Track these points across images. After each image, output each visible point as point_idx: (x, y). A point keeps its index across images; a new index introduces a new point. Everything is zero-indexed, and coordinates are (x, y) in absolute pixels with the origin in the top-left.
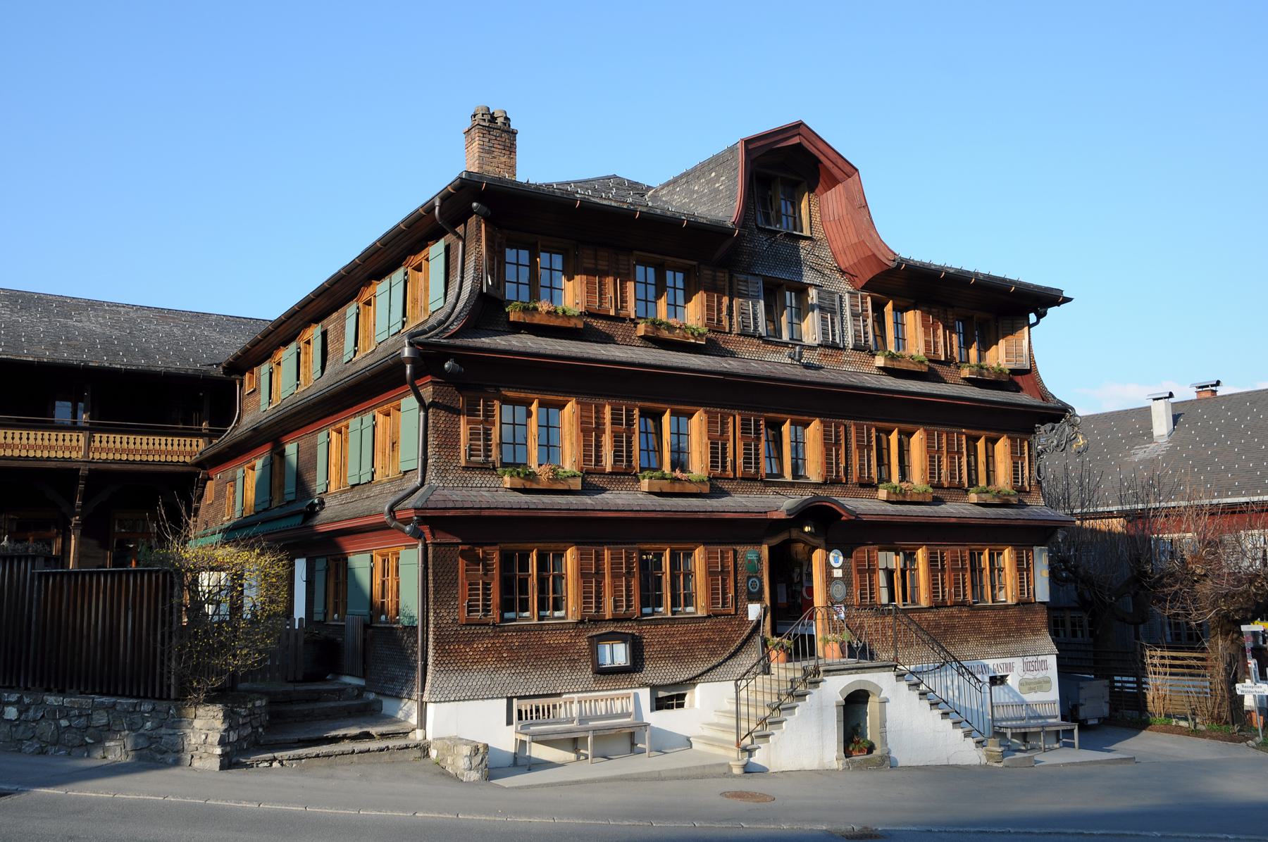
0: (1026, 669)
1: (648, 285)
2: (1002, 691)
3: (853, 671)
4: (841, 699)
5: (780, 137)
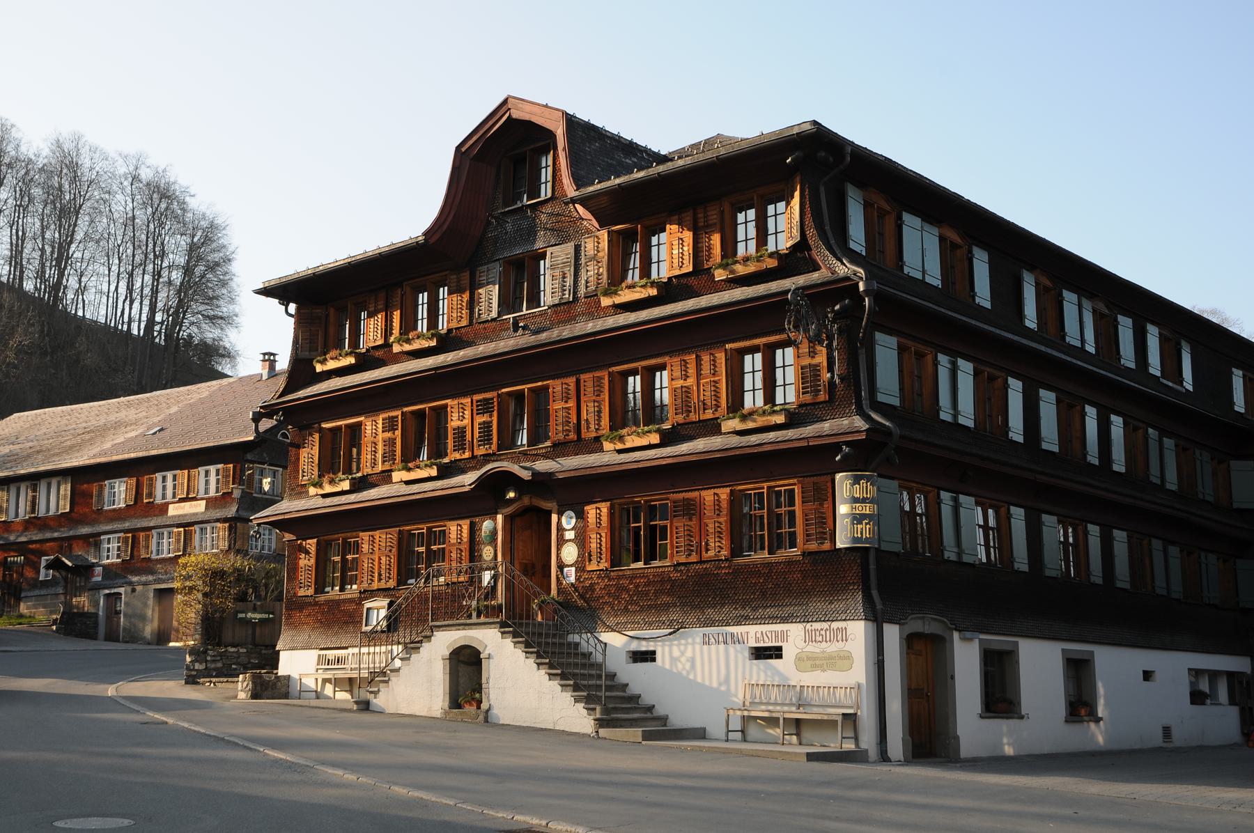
0: (810, 638)
1: (774, 217)
2: (755, 668)
3: (461, 627)
4: (447, 653)
5: (491, 123)
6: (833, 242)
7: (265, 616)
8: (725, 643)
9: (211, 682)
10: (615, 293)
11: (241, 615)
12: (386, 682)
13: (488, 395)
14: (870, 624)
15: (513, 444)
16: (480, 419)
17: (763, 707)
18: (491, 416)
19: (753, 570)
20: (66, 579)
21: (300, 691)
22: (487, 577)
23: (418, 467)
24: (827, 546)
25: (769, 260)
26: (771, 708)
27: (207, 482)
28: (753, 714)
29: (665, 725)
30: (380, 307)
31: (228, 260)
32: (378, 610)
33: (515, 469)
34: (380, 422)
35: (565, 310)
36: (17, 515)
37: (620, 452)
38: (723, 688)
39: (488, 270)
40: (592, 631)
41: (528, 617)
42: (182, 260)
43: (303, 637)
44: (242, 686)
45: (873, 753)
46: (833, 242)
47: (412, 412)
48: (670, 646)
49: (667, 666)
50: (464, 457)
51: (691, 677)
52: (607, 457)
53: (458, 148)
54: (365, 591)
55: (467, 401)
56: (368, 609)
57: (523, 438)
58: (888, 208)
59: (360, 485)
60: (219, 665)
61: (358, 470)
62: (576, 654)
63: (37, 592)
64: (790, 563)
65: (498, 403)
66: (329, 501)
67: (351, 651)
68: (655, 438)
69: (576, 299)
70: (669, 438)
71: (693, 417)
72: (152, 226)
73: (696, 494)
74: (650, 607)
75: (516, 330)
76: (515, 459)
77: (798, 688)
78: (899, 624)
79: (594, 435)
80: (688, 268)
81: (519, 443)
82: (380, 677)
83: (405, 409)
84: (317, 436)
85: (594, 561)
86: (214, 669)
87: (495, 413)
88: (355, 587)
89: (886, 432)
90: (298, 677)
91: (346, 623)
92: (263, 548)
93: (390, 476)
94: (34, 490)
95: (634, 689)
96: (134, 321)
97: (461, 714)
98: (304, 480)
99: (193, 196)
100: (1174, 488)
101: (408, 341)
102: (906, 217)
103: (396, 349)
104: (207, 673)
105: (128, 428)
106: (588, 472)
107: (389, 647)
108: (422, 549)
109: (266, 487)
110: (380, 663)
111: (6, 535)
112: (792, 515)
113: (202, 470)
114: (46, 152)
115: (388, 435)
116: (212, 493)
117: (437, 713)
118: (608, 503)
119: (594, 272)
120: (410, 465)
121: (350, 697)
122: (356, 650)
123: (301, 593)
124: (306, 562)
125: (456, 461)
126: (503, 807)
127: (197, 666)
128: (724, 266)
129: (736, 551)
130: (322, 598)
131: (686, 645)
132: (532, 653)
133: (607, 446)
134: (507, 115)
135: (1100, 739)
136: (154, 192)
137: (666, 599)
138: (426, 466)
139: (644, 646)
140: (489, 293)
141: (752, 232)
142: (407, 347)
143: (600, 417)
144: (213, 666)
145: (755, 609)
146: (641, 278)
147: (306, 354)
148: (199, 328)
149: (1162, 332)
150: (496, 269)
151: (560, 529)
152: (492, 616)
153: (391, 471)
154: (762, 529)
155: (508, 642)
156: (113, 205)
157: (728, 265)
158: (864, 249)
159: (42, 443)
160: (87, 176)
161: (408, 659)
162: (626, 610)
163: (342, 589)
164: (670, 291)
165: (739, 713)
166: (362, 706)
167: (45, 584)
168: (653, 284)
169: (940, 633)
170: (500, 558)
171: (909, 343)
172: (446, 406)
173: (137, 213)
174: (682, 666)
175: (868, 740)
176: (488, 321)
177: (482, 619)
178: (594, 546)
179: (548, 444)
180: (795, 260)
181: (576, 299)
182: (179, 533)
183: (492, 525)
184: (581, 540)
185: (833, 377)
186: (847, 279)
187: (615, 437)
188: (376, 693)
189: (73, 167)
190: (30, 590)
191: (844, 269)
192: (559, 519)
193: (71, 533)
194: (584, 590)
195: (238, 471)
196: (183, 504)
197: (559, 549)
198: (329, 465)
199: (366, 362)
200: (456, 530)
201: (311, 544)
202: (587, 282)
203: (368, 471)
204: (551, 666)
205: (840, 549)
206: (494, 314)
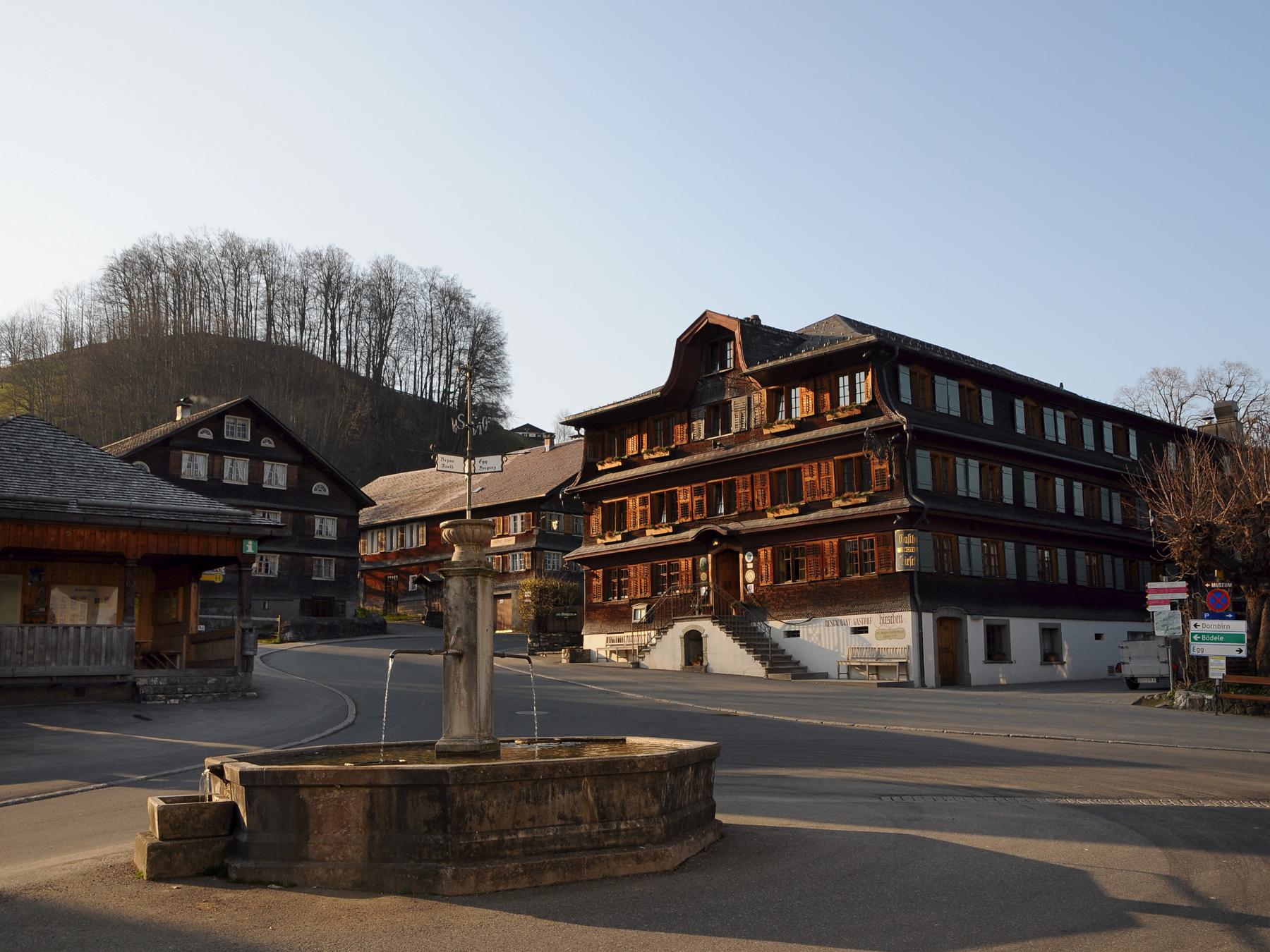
0: (883, 622)
2: (853, 639)
5: (697, 325)
6: (890, 400)
7: (572, 614)
8: (837, 625)
9: (543, 654)
10: (771, 427)
11: (559, 614)
12: (649, 651)
13: (701, 485)
14: (914, 613)
15: (716, 513)
16: (696, 499)
17: (858, 660)
18: (703, 497)
19: (851, 584)
20: (426, 590)
21: (598, 658)
22: (703, 590)
23: (661, 527)
24: (891, 571)
25: (855, 410)
26: (862, 660)
27: (515, 525)
28: (852, 664)
29: (806, 672)
30: (635, 432)
31: (501, 344)
32: (641, 612)
33: (717, 529)
34: (638, 500)
35: (743, 436)
36: (392, 548)
37: (777, 518)
38: (837, 650)
39: (698, 411)
40: (763, 620)
41: (727, 614)
42: (468, 346)
43: (597, 627)
44: (564, 655)
45: (917, 682)
46: (890, 400)
47: (657, 494)
48: (807, 628)
49: (806, 639)
50: (688, 521)
51: (819, 645)
52: (770, 521)
53: (678, 340)
54: (633, 599)
55: (688, 488)
56: (635, 610)
57: (722, 509)
58: (927, 374)
59: (626, 538)
60: (547, 644)
61: (626, 528)
62: (754, 634)
63: (408, 599)
64: (872, 580)
65: (707, 490)
66: (609, 547)
67: (625, 634)
68: (796, 511)
69: (749, 429)
70: (804, 511)
71: (817, 498)
72: (445, 322)
73: (820, 541)
74: (796, 606)
75: (715, 447)
76: (718, 522)
77: (877, 649)
78: (933, 612)
79: (762, 508)
80: (812, 413)
81: (719, 512)
82: (644, 649)
83: (652, 492)
84: (600, 508)
85: (764, 581)
86: (545, 646)
87: (705, 495)
88: (626, 597)
89: (922, 508)
90: (596, 650)
91: (623, 618)
92: (553, 567)
93: (645, 532)
94: (402, 532)
95: (789, 652)
96: (435, 391)
97: (692, 668)
98: (593, 534)
99: (474, 297)
100: (1120, 522)
101: (653, 453)
102: (937, 378)
103: (646, 457)
104: (540, 649)
105: (460, 488)
106: (759, 530)
107: (649, 632)
108: (665, 575)
109: (555, 527)
110: (644, 640)
111: (385, 562)
112: (872, 553)
113: (511, 516)
114: (369, 271)
115: (643, 508)
116: (519, 532)
117: (678, 668)
118: (771, 547)
119: (759, 414)
120: (657, 526)
121: (626, 661)
122: (630, 634)
123: (595, 601)
124: (597, 583)
125: (683, 523)
126: (716, 706)
127: (534, 645)
128: (832, 413)
129: (842, 574)
130: (607, 603)
131: (816, 627)
132: (730, 633)
133: (769, 515)
134: (706, 321)
135: (1065, 675)
136: (446, 296)
137: (805, 601)
138: (666, 526)
139: (793, 628)
140: (699, 424)
141: (847, 393)
142: (652, 456)
143: (765, 498)
144: (544, 644)
145: (853, 606)
146: (786, 419)
147: (591, 460)
148: (482, 395)
149: (1114, 424)
150: (703, 410)
151: (745, 563)
152: (708, 614)
153: (646, 529)
154: (857, 562)
155: (717, 627)
156: (417, 307)
157: (833, 412)
158: (910, 401)
159: (403, 499)
160: (397, 285)
161: (661, 638)
162: (783, 608)
163: (619, 598)
164: (802, 425)
165: (844, 663)
166: (636, 666)
167: (413, 593)
168: (792, 422)
169: (959, 616)
170: (710, 580)
171: (936, 452)
172: (676, 490)
173: (435, 312)
174: (814, 639)
175: (914, 675)
176: (699, 441)
177: (702, 615)
178: (764, 572)
179: (736, 513)
180: (869, 411)
181: (749, 429)
182: (499, 558)
183: (706, 560)
184: (757, 569)
185: (892, 477)
186: (897, 422)
187: (774, 510)
188: (643, 658)
189: (388, 281)
190: (403, 598)
191: (897, 416)
192: (744, 557)
193: (427, 560)
194: (758, 596)
195: (536, 518)
196: (499, 539)
197: (744, 574)
198: (607, 527)
199: (627, 465)
200: (685, 563)
201: (599, 572)
202: (755, 419)
203: (631, 529)
204: (741, 640)
205: (898, 572)
206: (702, 437)
